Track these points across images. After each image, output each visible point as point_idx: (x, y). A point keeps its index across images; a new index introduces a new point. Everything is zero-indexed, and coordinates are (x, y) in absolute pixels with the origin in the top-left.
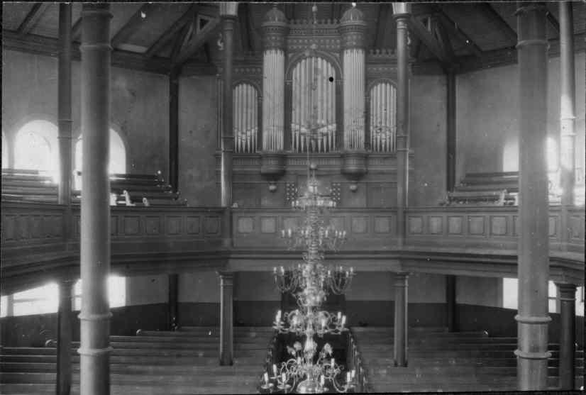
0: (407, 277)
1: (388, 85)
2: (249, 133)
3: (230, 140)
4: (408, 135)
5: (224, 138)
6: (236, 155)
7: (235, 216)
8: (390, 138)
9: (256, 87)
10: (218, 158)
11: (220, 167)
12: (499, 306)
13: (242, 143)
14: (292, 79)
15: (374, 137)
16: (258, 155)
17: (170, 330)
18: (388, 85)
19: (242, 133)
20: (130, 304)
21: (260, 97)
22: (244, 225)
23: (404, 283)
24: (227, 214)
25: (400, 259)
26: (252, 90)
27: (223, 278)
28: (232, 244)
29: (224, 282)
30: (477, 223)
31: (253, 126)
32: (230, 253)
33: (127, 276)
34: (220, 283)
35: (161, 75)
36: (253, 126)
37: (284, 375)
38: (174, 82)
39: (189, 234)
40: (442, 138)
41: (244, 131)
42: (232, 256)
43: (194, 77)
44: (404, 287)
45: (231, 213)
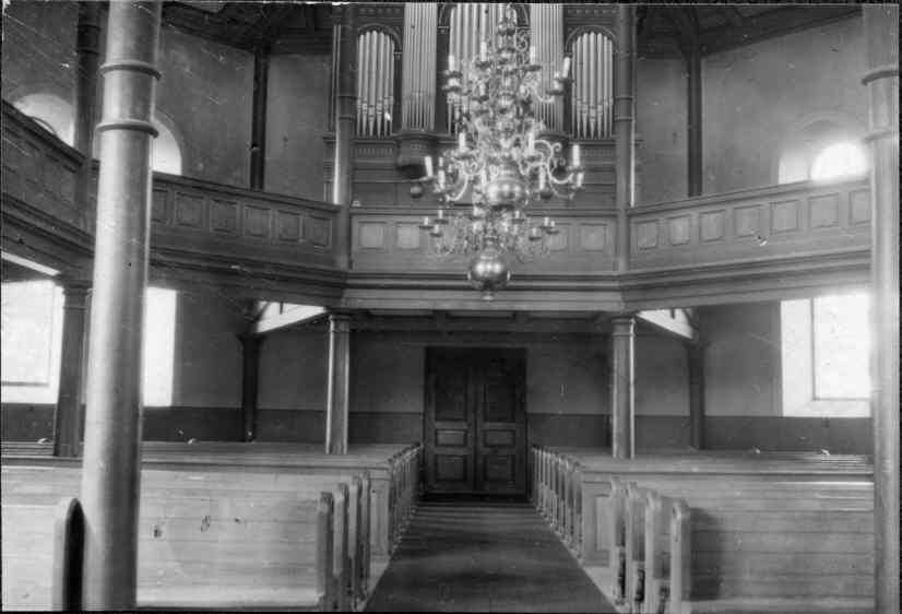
0: (633, 321)
1: (600, 36)
2: (386, 102)
3: (352, 122)
4: (633, 118)
5: (341, 118)
6: (360, 141)
7: (355, 221)
8: (603, 117)
9: (392, 37)
10: (330, 143)
11: (333, 156)
12: (776, 414)
13: (368, 122)
14: (448, 24)
15: (579, 109)
16: (394, 138)
17: (243, 441)
18: (600, 36)
19: (369, 106)
20: (179, 404)
21: (399, 48)
22: (370, 235)
23: (628, 330)
24: (342, 218)
25: (620, 290)
26: (385, 40)
27: (335, 320)
28: (350, 264)
29: (336, 327)
30: (746, 220)
31: (386, 95)
32: (346, 275)
33: (177, 289)
34: (329, 327)
35: (245, 52)
36: (386, 95)
37: (442, 174)
38: (262, 61)
39: (281, 239)
40: (682, 152)
41: (373, 103)
42: (350, 282)
43: (296, 56)
44: (628, 336)
45: (350, 216)
